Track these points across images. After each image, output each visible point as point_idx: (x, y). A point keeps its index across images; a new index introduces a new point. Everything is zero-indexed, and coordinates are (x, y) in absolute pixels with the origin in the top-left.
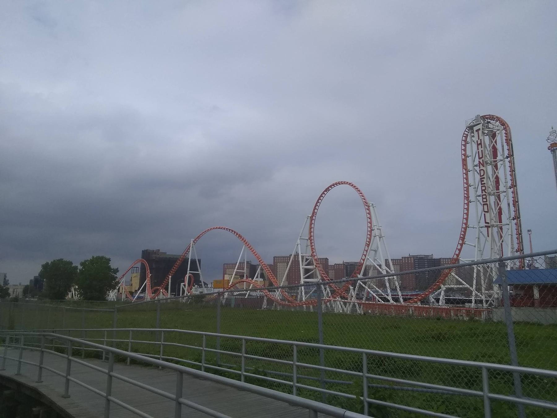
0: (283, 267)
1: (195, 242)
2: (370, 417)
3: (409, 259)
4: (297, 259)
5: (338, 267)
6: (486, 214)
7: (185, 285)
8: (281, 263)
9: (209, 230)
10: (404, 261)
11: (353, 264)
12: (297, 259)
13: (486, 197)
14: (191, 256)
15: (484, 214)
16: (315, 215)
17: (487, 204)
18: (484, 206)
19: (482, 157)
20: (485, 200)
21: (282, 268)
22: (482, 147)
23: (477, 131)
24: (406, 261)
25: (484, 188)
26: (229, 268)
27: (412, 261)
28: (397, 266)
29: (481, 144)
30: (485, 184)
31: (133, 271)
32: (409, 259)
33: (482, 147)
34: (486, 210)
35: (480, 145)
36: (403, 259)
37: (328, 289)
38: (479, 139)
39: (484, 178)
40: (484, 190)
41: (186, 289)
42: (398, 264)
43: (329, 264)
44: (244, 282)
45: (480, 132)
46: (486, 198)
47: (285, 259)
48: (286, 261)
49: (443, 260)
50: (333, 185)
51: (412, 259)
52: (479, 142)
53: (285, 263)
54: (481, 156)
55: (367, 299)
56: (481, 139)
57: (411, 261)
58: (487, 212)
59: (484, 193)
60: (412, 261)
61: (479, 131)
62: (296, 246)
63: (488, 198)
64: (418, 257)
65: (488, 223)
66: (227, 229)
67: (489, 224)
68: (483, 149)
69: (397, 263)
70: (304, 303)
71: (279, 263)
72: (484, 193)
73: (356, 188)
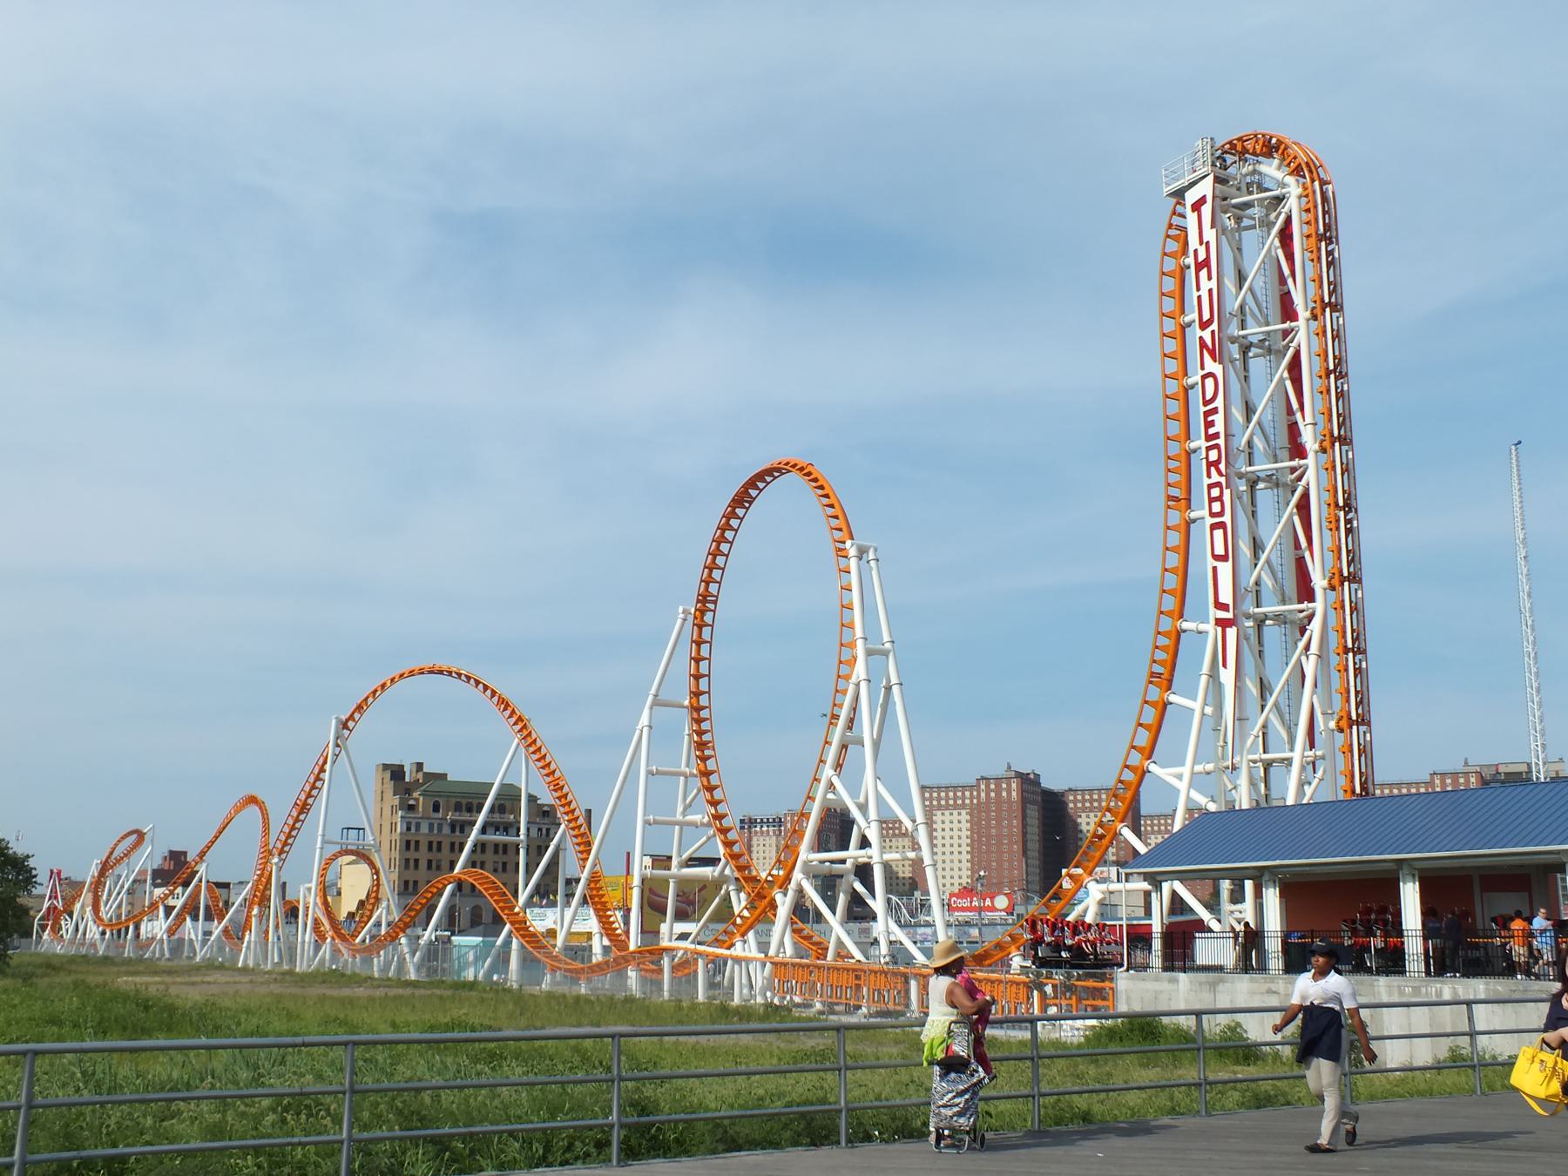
0: (955, 825)
3: (1004, 786)
4: (1004, 794)
5: (993, 794)
6: (1220, 565)
8: (947, 813)
9: (376, 691)
10: (983, 795)
11: (1521, 773)
12: (1004, 794)
13: (1222, 492)
15: (1215, 569)
16: (711, 606)
17: (1222, 525)
18: (1215, 532)
19: (1210, 322)
21: (951, 830)
23: (1197, 207)
24: (993, 794)
27: (1014, 794)
28: (951, 814)
30: (1216, 436)
33: (1210, 278)
35: (1205, 269)
36: (983, 787)
38: (1201, 243)
39: (1215, 411)
40: (1216, 464)
42: (963, 806)
43: (965, 816)
44: (116, 924)
45: (1207, 210)
46: (1220, 499)
47: (955, 794)
48: (967, 801)
49: (1091, 796)
53: (963, 812)
56: (1208, 243)
57: (1009, 793)
58: (1224, 558)
60: (1014, 794)
61: (1203, 208)
64: (1502, 769)
65: (1224, 607)
67: (1228, 610)
71: (939, 813)
73: (812, 477)
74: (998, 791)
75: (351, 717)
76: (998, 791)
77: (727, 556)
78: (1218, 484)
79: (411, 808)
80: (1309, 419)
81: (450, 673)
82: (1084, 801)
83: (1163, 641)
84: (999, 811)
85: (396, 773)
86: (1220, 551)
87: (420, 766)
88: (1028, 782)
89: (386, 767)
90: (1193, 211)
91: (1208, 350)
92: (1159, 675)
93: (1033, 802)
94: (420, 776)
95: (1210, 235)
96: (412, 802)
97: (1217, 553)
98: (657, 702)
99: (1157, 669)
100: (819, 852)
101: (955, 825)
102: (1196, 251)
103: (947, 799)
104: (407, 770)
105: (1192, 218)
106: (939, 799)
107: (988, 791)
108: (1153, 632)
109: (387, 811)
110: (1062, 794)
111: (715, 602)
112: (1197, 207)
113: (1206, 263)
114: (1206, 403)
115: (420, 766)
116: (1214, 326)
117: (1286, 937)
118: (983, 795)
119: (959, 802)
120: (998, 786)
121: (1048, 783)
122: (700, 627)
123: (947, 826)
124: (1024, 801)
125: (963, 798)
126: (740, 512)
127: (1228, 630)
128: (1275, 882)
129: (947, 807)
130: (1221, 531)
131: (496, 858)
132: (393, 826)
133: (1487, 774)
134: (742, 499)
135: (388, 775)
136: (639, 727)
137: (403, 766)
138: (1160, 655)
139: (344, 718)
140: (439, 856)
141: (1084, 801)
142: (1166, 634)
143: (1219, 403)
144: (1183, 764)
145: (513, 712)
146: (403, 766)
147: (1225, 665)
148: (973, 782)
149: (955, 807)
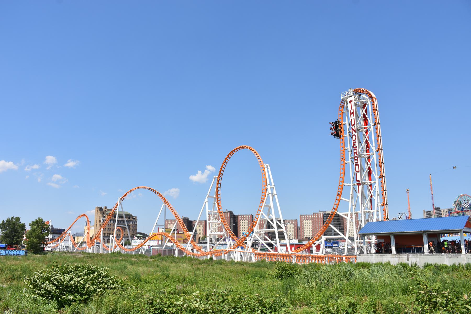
1: (122, 199)
2: (59, 228)
3: (319, 215)
4: (226, 216)
7: (113, 237)
10: (314, 216)
12: (226, 216)
14: (118, 212)
16: (221, 176)
19: (354, 125)
20: (356, 161)
22: (354, 116)
23: (351, 102)
24: (317, 216)
25: (355, 151)
26: (170, 223)
27: (228, 216)
29: (353, 113)
30: (356, 147)
31: (86, 225)
32: (319, 215)
33: (354, 116)
34: (357, 167)
37: (231, 241)
38: (352, 109)
40: (356, 153)
41: (114, 240)
43: (310, 221)
45: (353, 103)
46: (357, 160)
50: (236, 149)
51: (321, 214)
52: (352, 111)
54: (353, 123)
55: (261, 250)
58: (358, 171)
59: (356, 155)
60: (228, 216)
61: (352, 103)
62: (204, 203)
63: (359, 159)
64: (326, 212)
65: (359, 181)
66: (152, 189)
68: (355, 117)
69: (307, 218)
70: (208, 254)
71: (305, 220)
72: (356, 155)
74: (318, 215)
75: (123, 198)
76: (318, 215)
77: (226, 165)
78: (357, 157)
79: (104, 217)
80: (374, 145)
81: (145, 188)
82: (242, 217)
83: (340, 187)
84: (318, 220)
85: (101, 209)
86: (357, 170)
87: (106, 207)
88: (231, 213)
89: (98, 207)
90: (349, 102)
91: (354, 130)
92: (339, 194)
93: (232, 218)
94: (106, 210)
95: (354, 107)
96: (104, 216)
97: (356, 170)
98: (209, 196)
99: (339, 193)
100: (267, 229)
101: (245, 223)
102: (350, 110)
103: (308, 217)
104: (103, 208)
105: (349, 104)
106: (306, 217)
107: (316, 216)
108: (338, 185)
109: (98, 217)
110: (237, 216)
111: (222, 175)
112: (351, 102)
113: (353, 113)
114: (353, 141)
115: (106, 207)
116: (355, 126)
117: (422, 245)
118: (314, 216)
119: (246, 218)
120: (225, 214)
121: (235, 214)
122: (218, 181)
123: (243, 223)
124: (230, 217)
125: (310, 217)
126: (230, 156)
127: (360, 186)
128: (426, 235)
129: (306, 219)
130: (358, 167)
131: (110, 228)
132: (100, 221)
133: (324, 213)
134: (231, 154)
135: (99, 209)
136: (205, 202)
137: (102, 207)
138: (340, 190)
139: (121, 198)
140: (108, 228)
141: (242, 217)
142: (341, 186)
143: (357, 141)
144: (348, 212)
145: (163, 198)
146: (102, 207)
147: (359, 193)
148: (312, 214)
149: (308, 219)
